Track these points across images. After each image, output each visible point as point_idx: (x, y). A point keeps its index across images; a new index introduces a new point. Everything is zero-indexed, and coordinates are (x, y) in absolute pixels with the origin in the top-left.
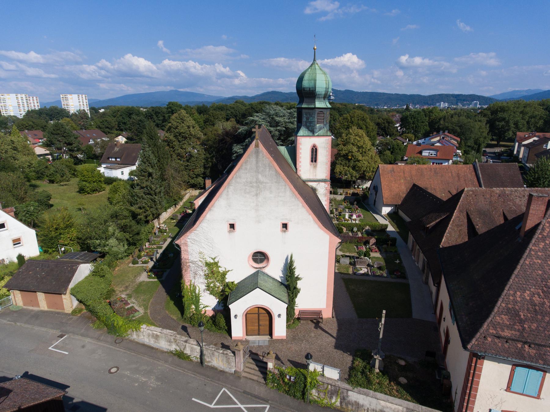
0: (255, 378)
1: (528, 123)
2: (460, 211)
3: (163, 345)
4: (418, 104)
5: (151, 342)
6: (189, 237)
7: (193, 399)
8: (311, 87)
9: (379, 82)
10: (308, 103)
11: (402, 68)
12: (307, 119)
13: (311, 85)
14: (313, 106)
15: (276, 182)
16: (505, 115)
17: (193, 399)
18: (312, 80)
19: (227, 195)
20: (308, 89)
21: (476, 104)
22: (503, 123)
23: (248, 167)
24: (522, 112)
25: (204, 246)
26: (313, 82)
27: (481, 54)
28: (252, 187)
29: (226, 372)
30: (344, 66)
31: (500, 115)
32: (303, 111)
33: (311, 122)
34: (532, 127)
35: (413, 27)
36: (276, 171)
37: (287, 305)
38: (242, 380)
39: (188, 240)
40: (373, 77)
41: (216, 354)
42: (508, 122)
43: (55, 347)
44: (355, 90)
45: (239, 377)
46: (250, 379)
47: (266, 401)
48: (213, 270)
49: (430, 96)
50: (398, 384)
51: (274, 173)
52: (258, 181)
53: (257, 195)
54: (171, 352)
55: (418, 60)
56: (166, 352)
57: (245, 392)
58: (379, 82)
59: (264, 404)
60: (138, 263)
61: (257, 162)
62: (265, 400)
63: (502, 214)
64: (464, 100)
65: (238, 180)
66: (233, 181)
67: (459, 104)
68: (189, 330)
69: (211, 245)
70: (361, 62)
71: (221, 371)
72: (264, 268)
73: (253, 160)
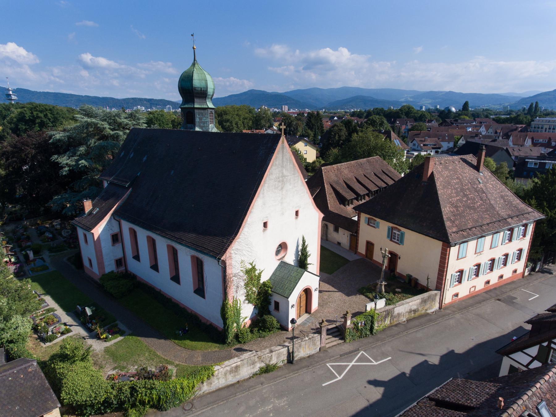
0: (335, 343)
1: (243, 122)
2: (327, 184)
3: (246, 372)
4: (114, 107)
5: (231, 379)
6: (233, 248)
7: (323, 385)
8: (202, 87)
9: (62, 81)
10: (200, 104)
11: (86, 67)
12: (200, 119)
13: (203, 85)
14: (205, 106)
15: (293, 174)
16: (228, 117)
17: (323, 385)
18: (202, 80)
19: (263, 194)
20: (200, 89)
21: (169, 108)
22: (228, 124)
23: (277, 163)
24: (237, 115)
25: (245, 254)
26: (204, 82)
27: (160, 62)
28: (279, 182)
29: (313, 355)
30: (8, 58)
31: (225, 117)
32: (196, 111)
33: (204, 123)
34: (246, 126)
35: (90, 23)
36: (294, 165)
37: (319, 278)
38: (329, 351)
39: (232, 252)
40: (53, 75)
41: (303, 343)
42: (231, 123)
43: (332, 366)
44: (33, 90)
45: (326, 351)
46: (332, 346)
47: (358, 350)
48: (251, 274)
49: (124, 100)
50: (399, 293)
51: (292, 166)
52: (283, 176)
53: (282, 189)
54: (255, 374)
55: (103, 61)
56: (250, 378)
57: (341, 356)
58: (62, 81)
59: (359, 353)
60: (57, 338)
61: (283, 156)
62: (356, 351)
63: (355, 180)
64: (157, 105)
65: (271, 177)
66: (268, 178)
67: (154, 108)
68: (245, 347)
69: (250, 250)
70: (31, 56)
71: (309, 357)
72: (284, 257)
73: (280, 156)
